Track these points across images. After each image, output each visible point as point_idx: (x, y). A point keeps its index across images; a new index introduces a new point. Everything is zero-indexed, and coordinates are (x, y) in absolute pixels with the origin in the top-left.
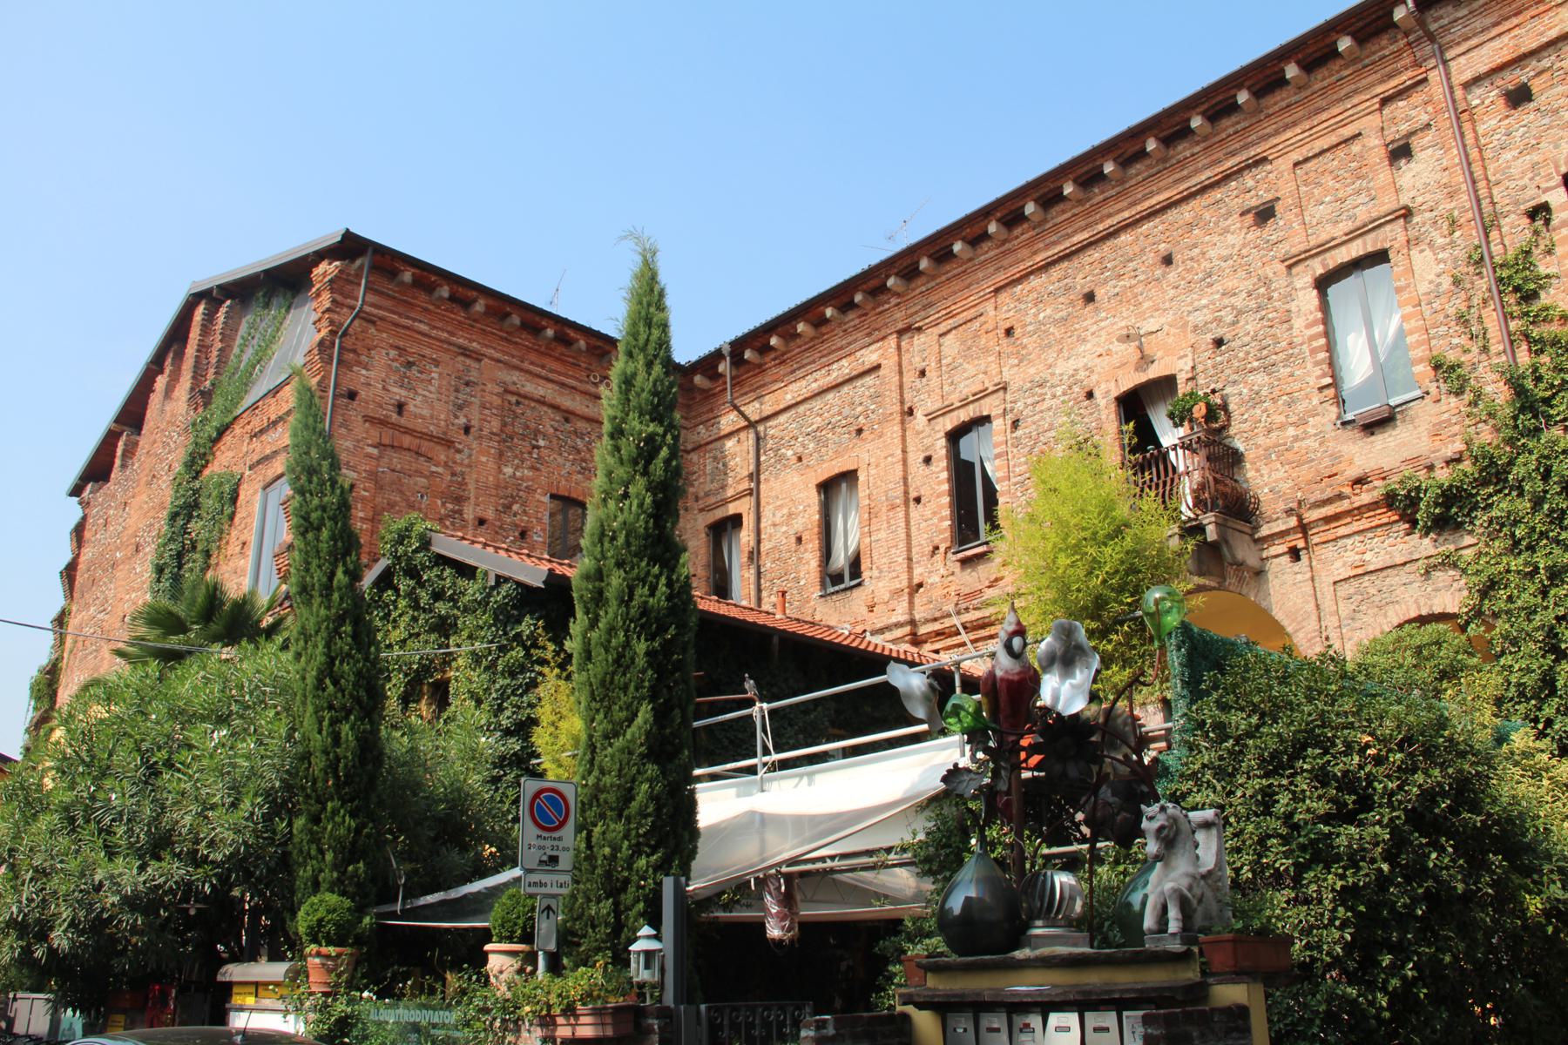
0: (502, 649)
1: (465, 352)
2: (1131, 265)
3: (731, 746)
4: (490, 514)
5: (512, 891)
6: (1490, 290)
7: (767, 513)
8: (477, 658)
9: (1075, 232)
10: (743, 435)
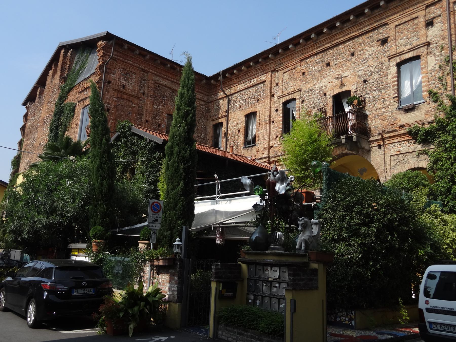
0: (150, 160)
1: (143, 70)
2: (342, 55)
3: (208, 192)
4: (150, 119)
5: (146, 227)
6: (450, 70)
7: (230, 122)
8: (143, 162)
9: (326, 44)
10: (225, 99)
